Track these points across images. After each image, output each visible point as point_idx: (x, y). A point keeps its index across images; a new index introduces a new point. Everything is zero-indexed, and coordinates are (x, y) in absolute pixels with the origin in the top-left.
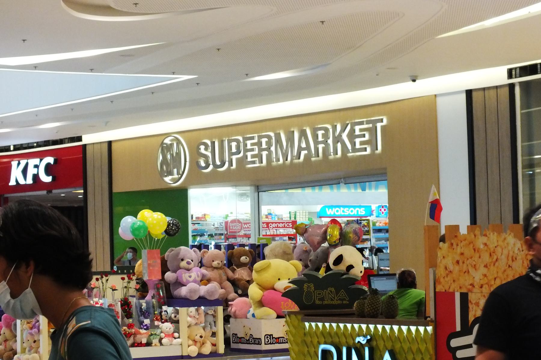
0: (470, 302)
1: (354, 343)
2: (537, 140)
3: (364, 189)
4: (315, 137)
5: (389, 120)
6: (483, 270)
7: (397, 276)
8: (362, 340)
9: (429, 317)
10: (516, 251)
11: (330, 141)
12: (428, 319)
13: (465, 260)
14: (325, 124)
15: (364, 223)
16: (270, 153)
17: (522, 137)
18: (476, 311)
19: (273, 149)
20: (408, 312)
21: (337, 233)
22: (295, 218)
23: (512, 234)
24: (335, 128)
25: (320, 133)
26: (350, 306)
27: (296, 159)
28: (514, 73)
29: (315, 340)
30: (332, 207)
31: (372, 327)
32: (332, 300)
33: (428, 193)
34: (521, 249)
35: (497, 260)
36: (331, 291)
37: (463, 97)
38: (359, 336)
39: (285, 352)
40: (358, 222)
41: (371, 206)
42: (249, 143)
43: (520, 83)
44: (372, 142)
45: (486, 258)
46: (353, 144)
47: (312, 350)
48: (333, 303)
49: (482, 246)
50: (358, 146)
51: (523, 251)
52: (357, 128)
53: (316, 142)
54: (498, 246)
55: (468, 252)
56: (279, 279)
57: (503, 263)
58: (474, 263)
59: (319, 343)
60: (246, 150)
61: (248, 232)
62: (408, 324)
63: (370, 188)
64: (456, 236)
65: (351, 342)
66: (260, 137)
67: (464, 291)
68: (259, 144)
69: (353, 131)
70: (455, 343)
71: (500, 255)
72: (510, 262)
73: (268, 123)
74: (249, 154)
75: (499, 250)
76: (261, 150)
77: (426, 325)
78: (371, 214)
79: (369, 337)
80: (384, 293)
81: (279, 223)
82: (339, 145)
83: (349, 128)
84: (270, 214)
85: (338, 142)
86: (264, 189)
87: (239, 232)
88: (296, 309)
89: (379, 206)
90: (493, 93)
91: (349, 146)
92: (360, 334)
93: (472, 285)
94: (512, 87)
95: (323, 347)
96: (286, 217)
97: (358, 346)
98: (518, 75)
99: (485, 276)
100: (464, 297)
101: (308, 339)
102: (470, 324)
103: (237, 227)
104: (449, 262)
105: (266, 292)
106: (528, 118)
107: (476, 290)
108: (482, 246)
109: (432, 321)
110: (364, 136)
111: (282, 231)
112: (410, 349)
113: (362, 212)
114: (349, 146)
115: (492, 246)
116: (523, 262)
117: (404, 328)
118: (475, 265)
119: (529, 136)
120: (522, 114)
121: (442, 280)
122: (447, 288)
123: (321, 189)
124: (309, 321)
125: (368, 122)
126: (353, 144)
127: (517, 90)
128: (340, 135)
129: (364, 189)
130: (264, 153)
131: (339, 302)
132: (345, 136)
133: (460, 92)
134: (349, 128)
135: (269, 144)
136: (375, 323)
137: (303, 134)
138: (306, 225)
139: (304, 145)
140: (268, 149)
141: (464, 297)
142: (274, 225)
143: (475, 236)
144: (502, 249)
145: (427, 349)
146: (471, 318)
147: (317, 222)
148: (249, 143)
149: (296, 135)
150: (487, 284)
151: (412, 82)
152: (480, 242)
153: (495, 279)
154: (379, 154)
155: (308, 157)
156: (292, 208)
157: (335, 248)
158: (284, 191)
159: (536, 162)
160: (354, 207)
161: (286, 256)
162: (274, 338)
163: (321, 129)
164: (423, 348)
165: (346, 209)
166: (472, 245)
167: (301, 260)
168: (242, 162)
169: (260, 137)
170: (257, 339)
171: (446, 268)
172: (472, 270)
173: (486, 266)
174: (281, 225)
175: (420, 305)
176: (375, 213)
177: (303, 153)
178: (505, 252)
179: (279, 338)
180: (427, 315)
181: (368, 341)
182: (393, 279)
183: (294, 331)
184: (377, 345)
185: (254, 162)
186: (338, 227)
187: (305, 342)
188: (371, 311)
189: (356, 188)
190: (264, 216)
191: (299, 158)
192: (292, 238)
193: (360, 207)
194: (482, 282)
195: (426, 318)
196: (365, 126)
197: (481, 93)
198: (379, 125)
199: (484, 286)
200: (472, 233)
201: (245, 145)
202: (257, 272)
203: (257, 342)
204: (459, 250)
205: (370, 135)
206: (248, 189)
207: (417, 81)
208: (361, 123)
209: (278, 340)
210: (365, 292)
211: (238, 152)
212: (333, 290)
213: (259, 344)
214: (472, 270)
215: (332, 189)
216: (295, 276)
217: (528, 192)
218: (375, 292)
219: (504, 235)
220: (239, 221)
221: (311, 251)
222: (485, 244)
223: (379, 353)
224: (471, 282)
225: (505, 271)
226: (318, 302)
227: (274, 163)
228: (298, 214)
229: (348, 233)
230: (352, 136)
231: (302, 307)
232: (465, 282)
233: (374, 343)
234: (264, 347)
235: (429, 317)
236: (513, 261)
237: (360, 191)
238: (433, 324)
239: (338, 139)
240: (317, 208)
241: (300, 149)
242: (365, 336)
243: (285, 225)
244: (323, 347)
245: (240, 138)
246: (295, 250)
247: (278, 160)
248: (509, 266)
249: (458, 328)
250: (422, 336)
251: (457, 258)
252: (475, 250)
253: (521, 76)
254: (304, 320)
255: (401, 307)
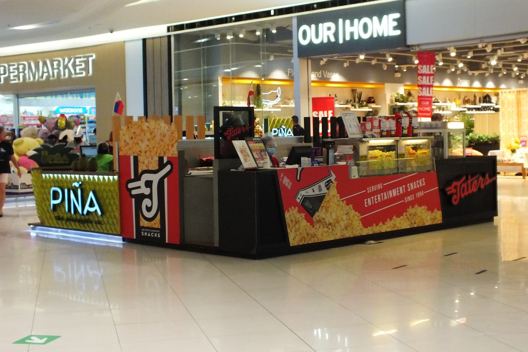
0: (139, 161)
1: (72, 186)
2: (183, 70)
3: (82, 97)
4: (52, 65)
5: (97, 56)
6: (147, 143)
7: (97, 146)
8: (76, 184)
9: (115, 170)
10: (166, 131)
11: (61, 68)
12: (115, 172)
13: (136, 136)
14: (58, 57)
15: (82, 117)
16: (25, 74)
17: (175, 68)
18: (143, 167)
19: (26, 72)
20: (104, 168)
21: (64, 122)
22: (41, 114)
23: (163, 121)
24: (64, 60)
25: (55, 63)
26: (69, 164)
27: (41, 78)
28: (170, 29)
29: (49, 185)
30: (63, 108)
31: (82, 176)
32: (58, 161)
33: (115, 96)
34: (168, 130)
35: (154, 137)
36: (58, 155)
37: (141, 43)
38: (75, 182)
39: (31, 193)
40: (78, 117)
41: (85, 108)
42: (11, 68)
43: (175, 35)
44: (86, 69)
45: (148, 135)
46: (75, 70)
47: (47, 191)
48: (59, 162)
49: (146, 128)
50: (78, 71)
51: (169, 131)
52: (78, 61)
53: (53, 69)
54: (155, 128)
55: (138, 131)
56: (29, 150)
57: (158, 138)
58: (142, 138)
59: (51, 187)
60: (10, 73)
61: (12, 123)
62: (103, 174)
63: (86, 97)
64: (131, 122)
65: (70, 186)
66: (19, 65)
67: (136, 155)
68: (18, 69)
69: (75, 62)
70: (131, 186)
71: (156, 133)
72: (162, 138)
73: (24, 56)
74: (12, 75)
75: (156, 130)
76: (19, 72)
77: (113, 175)
78: (86, 112)
79: (80, 183)
80: (89, 157)
81: (31, 117)
82: (67, 70)
83: (72, 60)
84: (26, 112)
85: (66, 69)
86: (22, 96)
87: (6, 122)
88: (37, 166)
89: (91, 108)
90: (158, 41)
91: (73, 71)
92: (75, 180)
93: (140, 151)
94: (169, 37)
95: (53, 189)
96: (35, 113)
97: (74, 188)
98: (173, 30)
99: (148, 146)
100: (136, 159)
101: (45, 184)
102: (139, 174)
103: (5, 119)
104: (127, 138)
105: (22, 157)
106: (178, 56)
107: (143, 154)
108: (146, 128)
109: (117, 173)
110: (81, 65)
111: (33, 122)
112: (105, 190)
113: (81, 111)
114: (73, 71)
115: (151, 128)
116: (169, 137)
117: (101, 177)
118: (142, 140)
119: (178, 68)
120: (175, 54)
121: (123, 149)
122: (126, 153)
123: (56, 97)
124: (45, 173)
125: (84, 57)
126: (75, 70)
127: (172, 39)
128: (67, 65)
129: (82, 97)
130: (21, 75)
131: (63, 162)
132: (70, 66)
133: (139, 40)
134: (72, 60)
135: (24, 69)
136: (84, 174)
137: (45, 63)
138: (45, 118)
139: (45, 70)
140: (24, 72)
141: (136, 159)
142: (28, 118)
143: (142, 122)
144: (158, 130)
145: (114, 190)
146: (140, 171)
147: (54, 116)
148: (11, 68)
149: (41, 64)
150: (148, 151)
151: (110, 33)
152: (145, 125)
153: (153, 148)
154: (90, 77)
155: (48, 77)
156: (39, 108)
157: (63, 131)
158: (33, 98)
159: (182, 83)
160: (76, 108)
161: (34, 136)
162: (26, 185)
163: (55, 60)
164: (112, 189)
165: (71, 109)
166: (140, 128)
167: (42, 138)
168: (7, 79)
169: (19, 65)
170: (16, 186)
171: (125, 141)
172: (139, 142)
173: (148, 140)
174: (32, 119)
175: (111, 163)
176: (88, 112)
177: (45, 75)
178: (159, 132)
179: (29, 185)
180: (114, 170)
181: (80, 185)
182: (95, 148)
183: (36, 179)
184: (85, 188)
185: (15, 80)
186: (64, 119)
187: (42, 187)
188: (81, 167)
189: (77, 97)
190: (22, 113)
191: (43, 78)
192: (38, 126)
193: (80, 108)
194: (146, 150)
195: (114, 171)
196: (82, 59)
197: (152, 40)
198: (90, 59)
199: (147, 152)
200: (140, 121)
201: (9, 70)
202: (16, 145)
203: (16, 187)
204: (133, 131)
205: (85, 64)
206: (11, 97)
207: (114, 33)
208: (80, 58)
209: (29, 187)
210: (78, 156)
211: (5, 73)
212: (59, 154)
213: (17, 188)
214: (139, 142)
215: (63, 97)
216: (38, 146)
217: (178, 101)
218: (84, 156)
219: (159, 122)
220: (6, 116)
221: (48, 133)
222: (148, 127)
223: (86, 192)
224: (140, 150)
225: (159, 143)
226: (50, 162)
227: (27, 81)
228: (43, 112)
229: (71, 122)
230: (74, 65)
231: (41, 165)
232: (136, 149)
233: (83, 186)
234: (20, 191)
235: (115, 170)
236: (164, 137)
237: (79, 98)
238: (117, 174)
239: (66, 67)
240: (55, 108)
241: (43, 73)
242: (78, 182)
243: (34, 118)
244: (53, 189)
245: (6, 65)
246: (40, 132)
247: (30, 79)
248: (162, 140)
249: (133, 177)
250: (112, 181)
251: (132, 135)
252: (142, 131)
253: (175, 31)
254: (42, 173)
255: (99, 165)
